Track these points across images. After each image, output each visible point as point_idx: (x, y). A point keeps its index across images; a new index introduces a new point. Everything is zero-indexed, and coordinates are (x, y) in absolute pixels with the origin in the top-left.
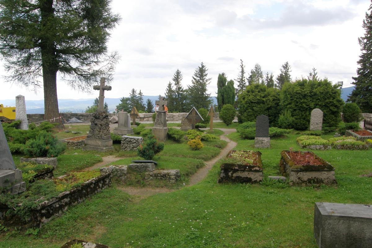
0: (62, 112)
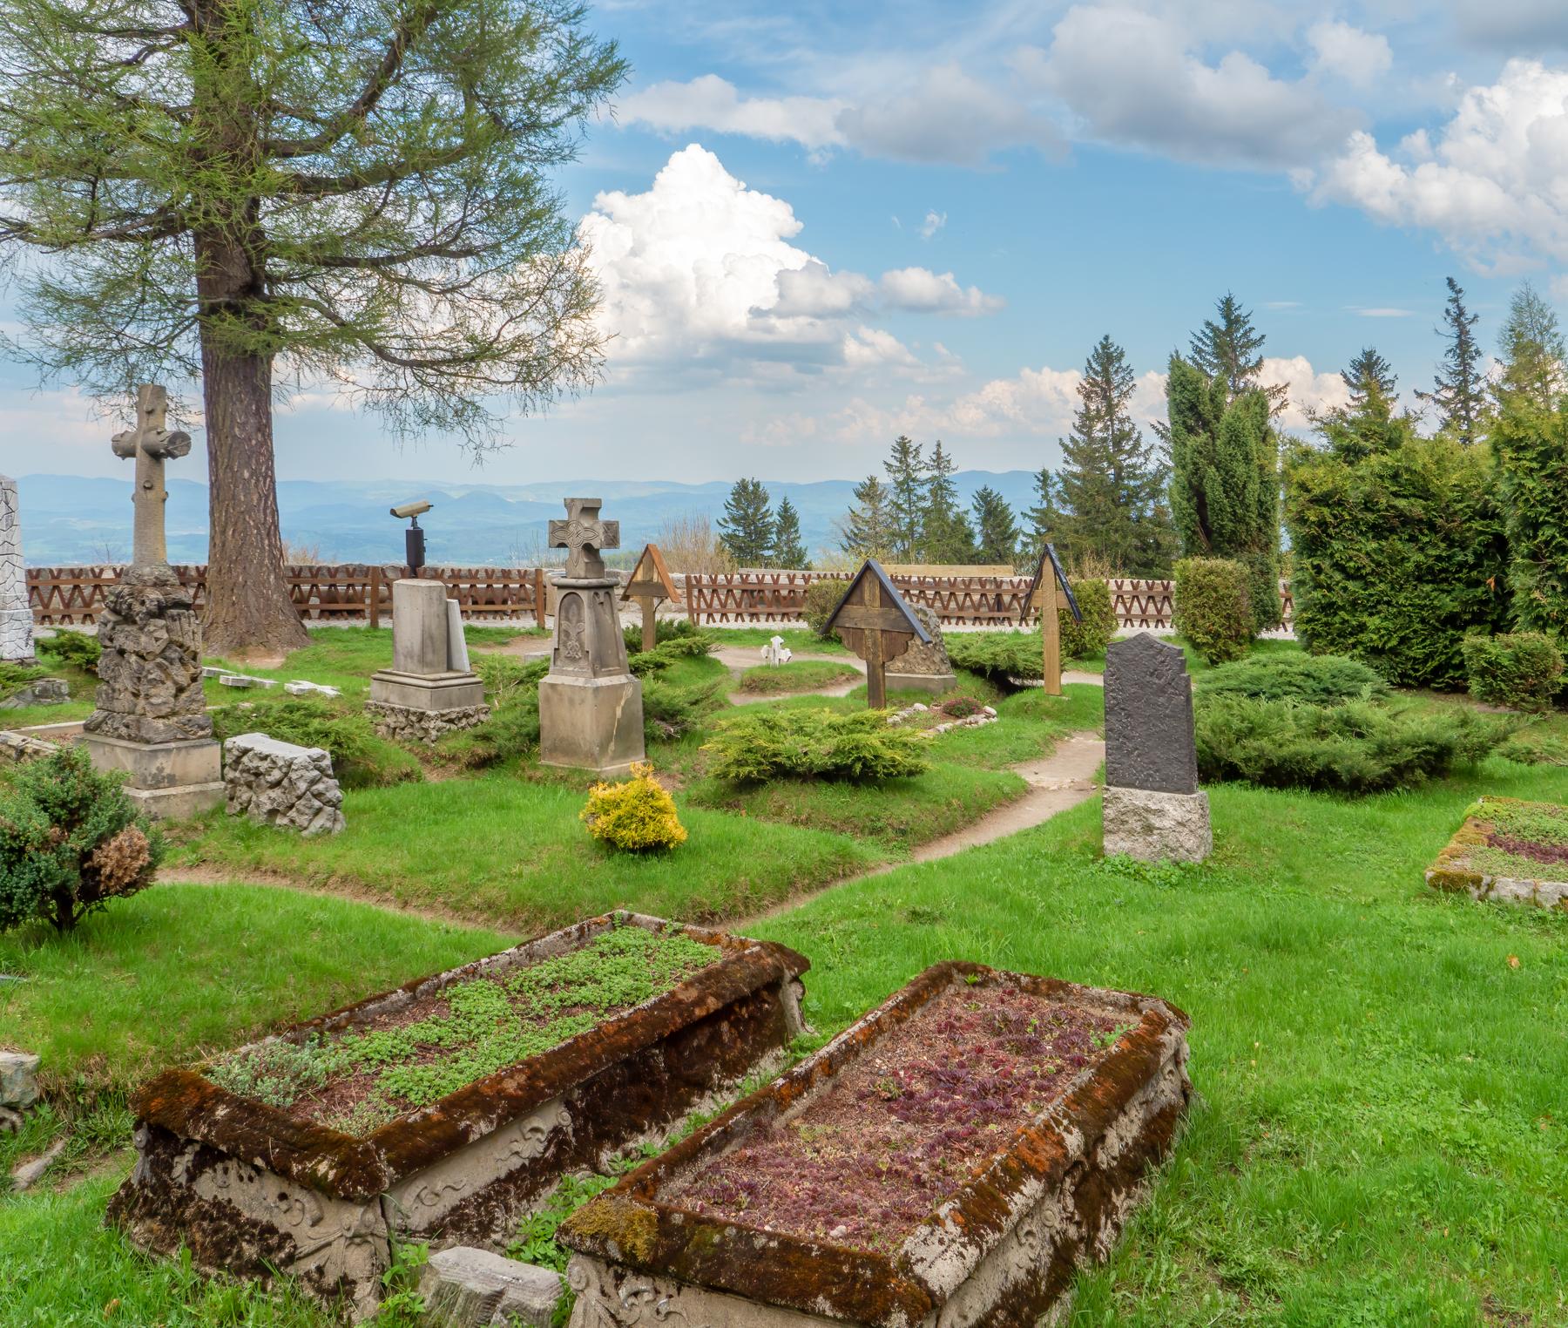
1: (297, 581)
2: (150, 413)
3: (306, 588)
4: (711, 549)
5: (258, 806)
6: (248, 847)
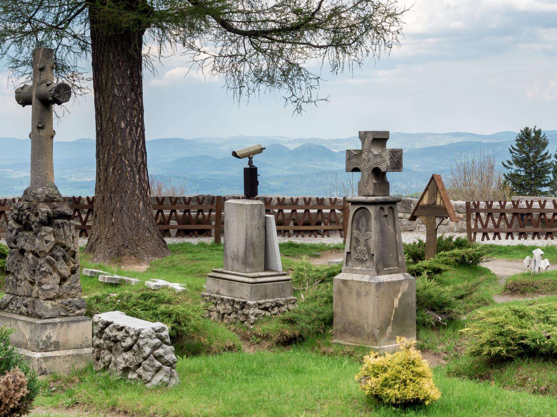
0: (165, 192)
1: (160, 207)
2: (42, 69)
3: (167, 213)
4: (494, 187)
5: (116, 365)
6: (107, 394)
